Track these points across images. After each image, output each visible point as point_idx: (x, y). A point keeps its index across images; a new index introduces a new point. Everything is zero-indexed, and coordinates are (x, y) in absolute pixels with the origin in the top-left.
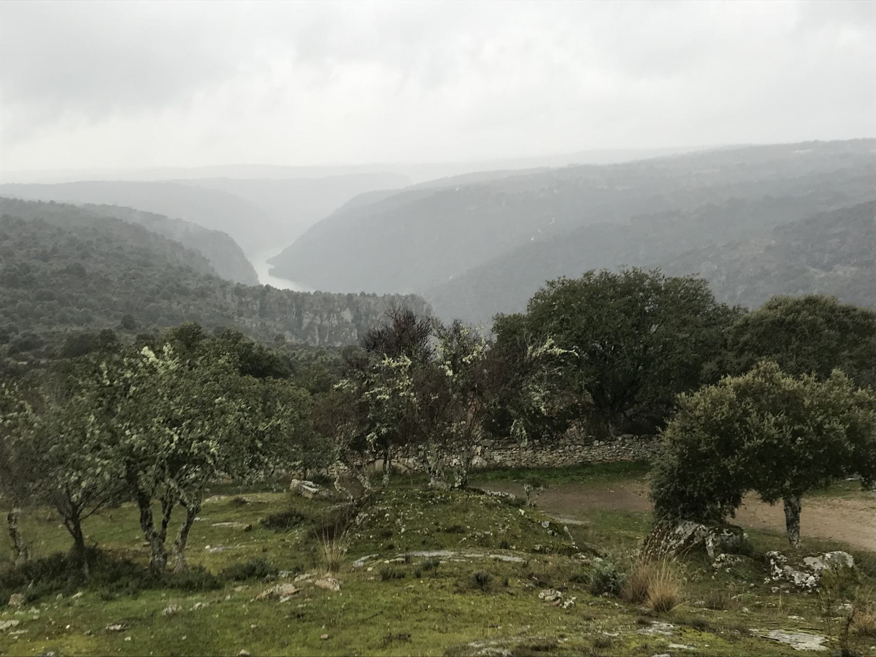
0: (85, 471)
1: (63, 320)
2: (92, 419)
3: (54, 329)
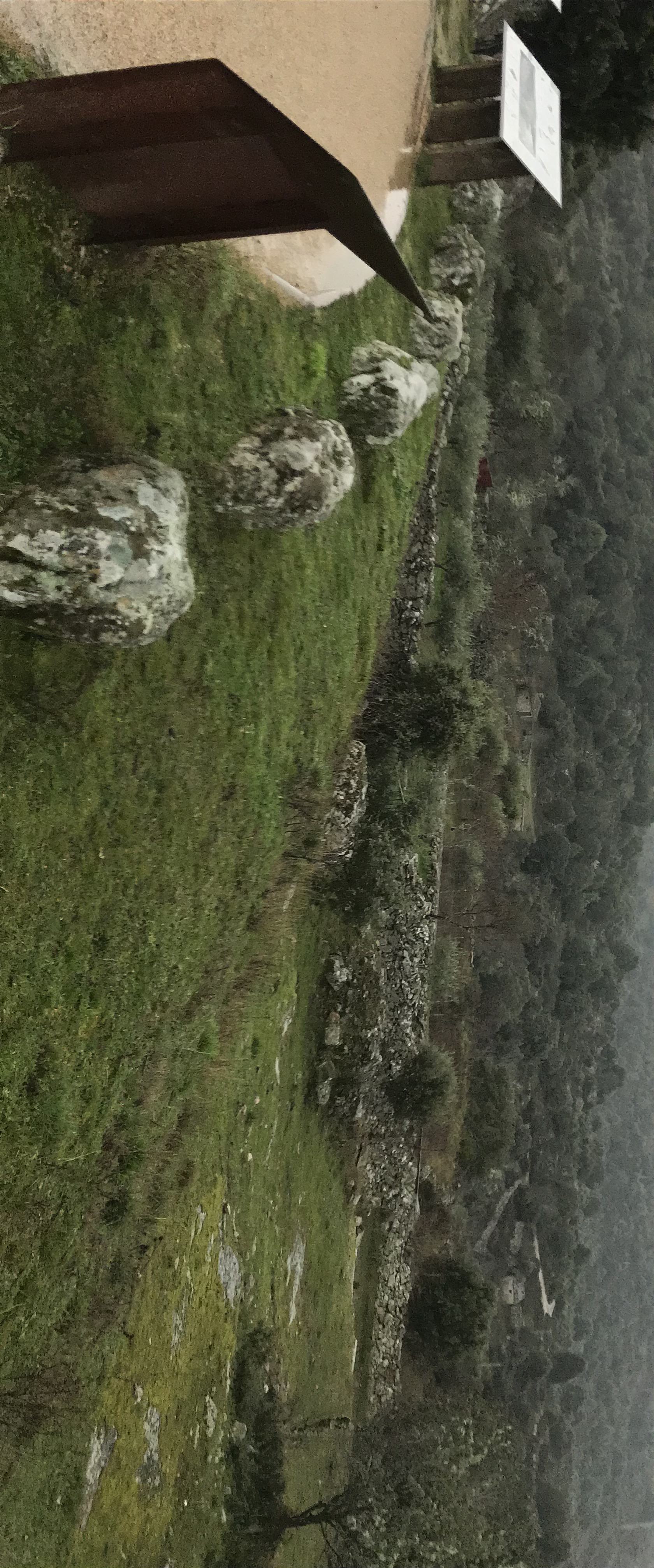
0: (385, 1536)
1: (585, 1487)
2: (452, 1551)
3: (576, 1473)
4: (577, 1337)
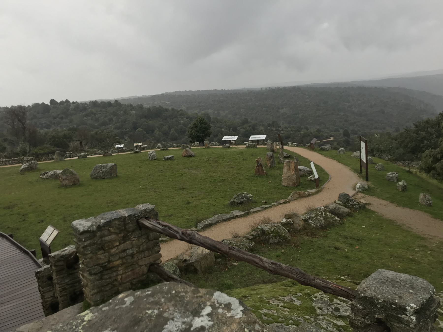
1: (376, 128)
4: (339, 131)
